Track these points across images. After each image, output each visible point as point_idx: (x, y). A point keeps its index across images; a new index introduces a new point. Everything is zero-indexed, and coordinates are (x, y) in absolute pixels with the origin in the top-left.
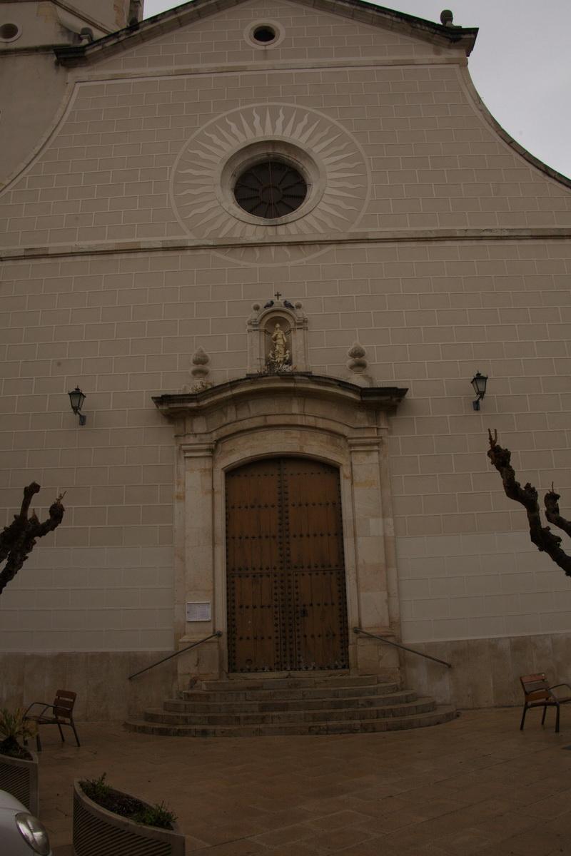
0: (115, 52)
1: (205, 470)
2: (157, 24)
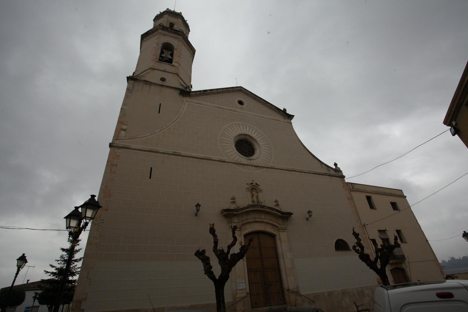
0: (198, 96)
1: (239, 235)
2: (212, 91)
